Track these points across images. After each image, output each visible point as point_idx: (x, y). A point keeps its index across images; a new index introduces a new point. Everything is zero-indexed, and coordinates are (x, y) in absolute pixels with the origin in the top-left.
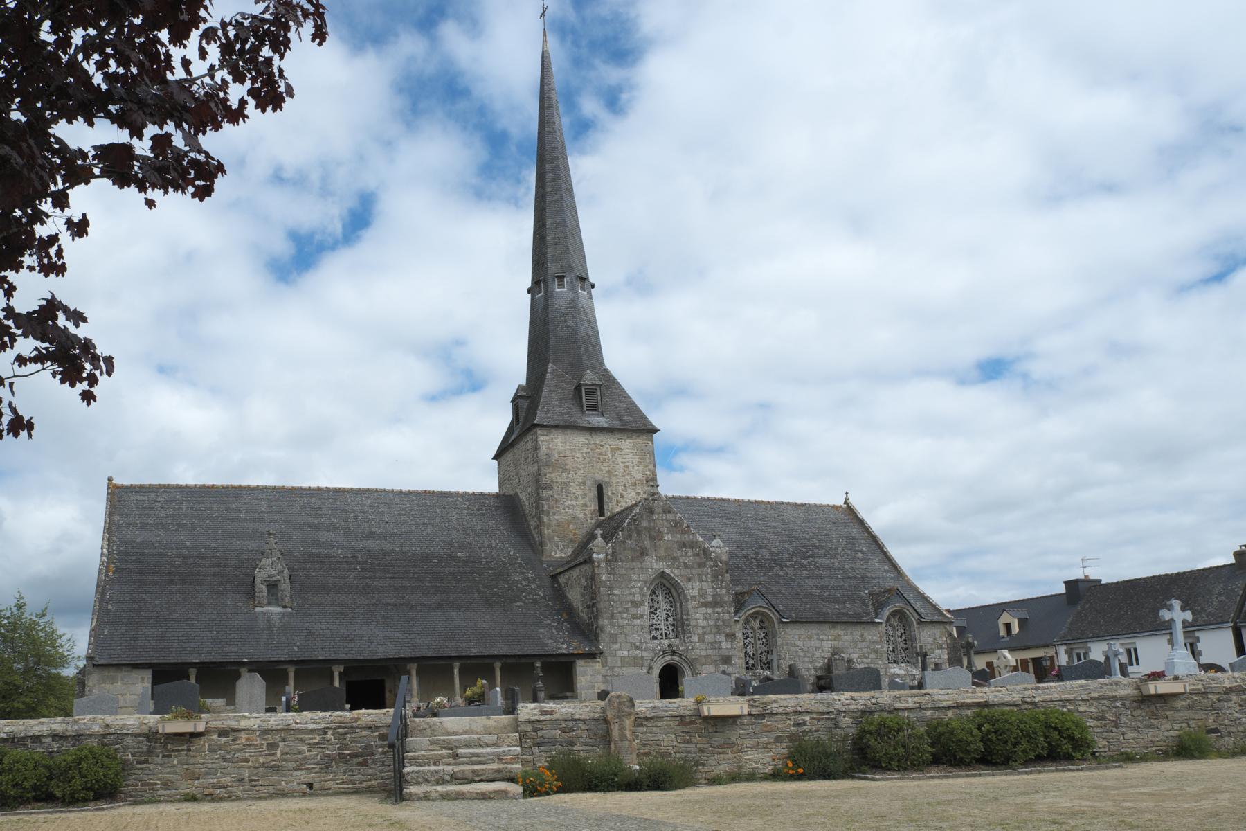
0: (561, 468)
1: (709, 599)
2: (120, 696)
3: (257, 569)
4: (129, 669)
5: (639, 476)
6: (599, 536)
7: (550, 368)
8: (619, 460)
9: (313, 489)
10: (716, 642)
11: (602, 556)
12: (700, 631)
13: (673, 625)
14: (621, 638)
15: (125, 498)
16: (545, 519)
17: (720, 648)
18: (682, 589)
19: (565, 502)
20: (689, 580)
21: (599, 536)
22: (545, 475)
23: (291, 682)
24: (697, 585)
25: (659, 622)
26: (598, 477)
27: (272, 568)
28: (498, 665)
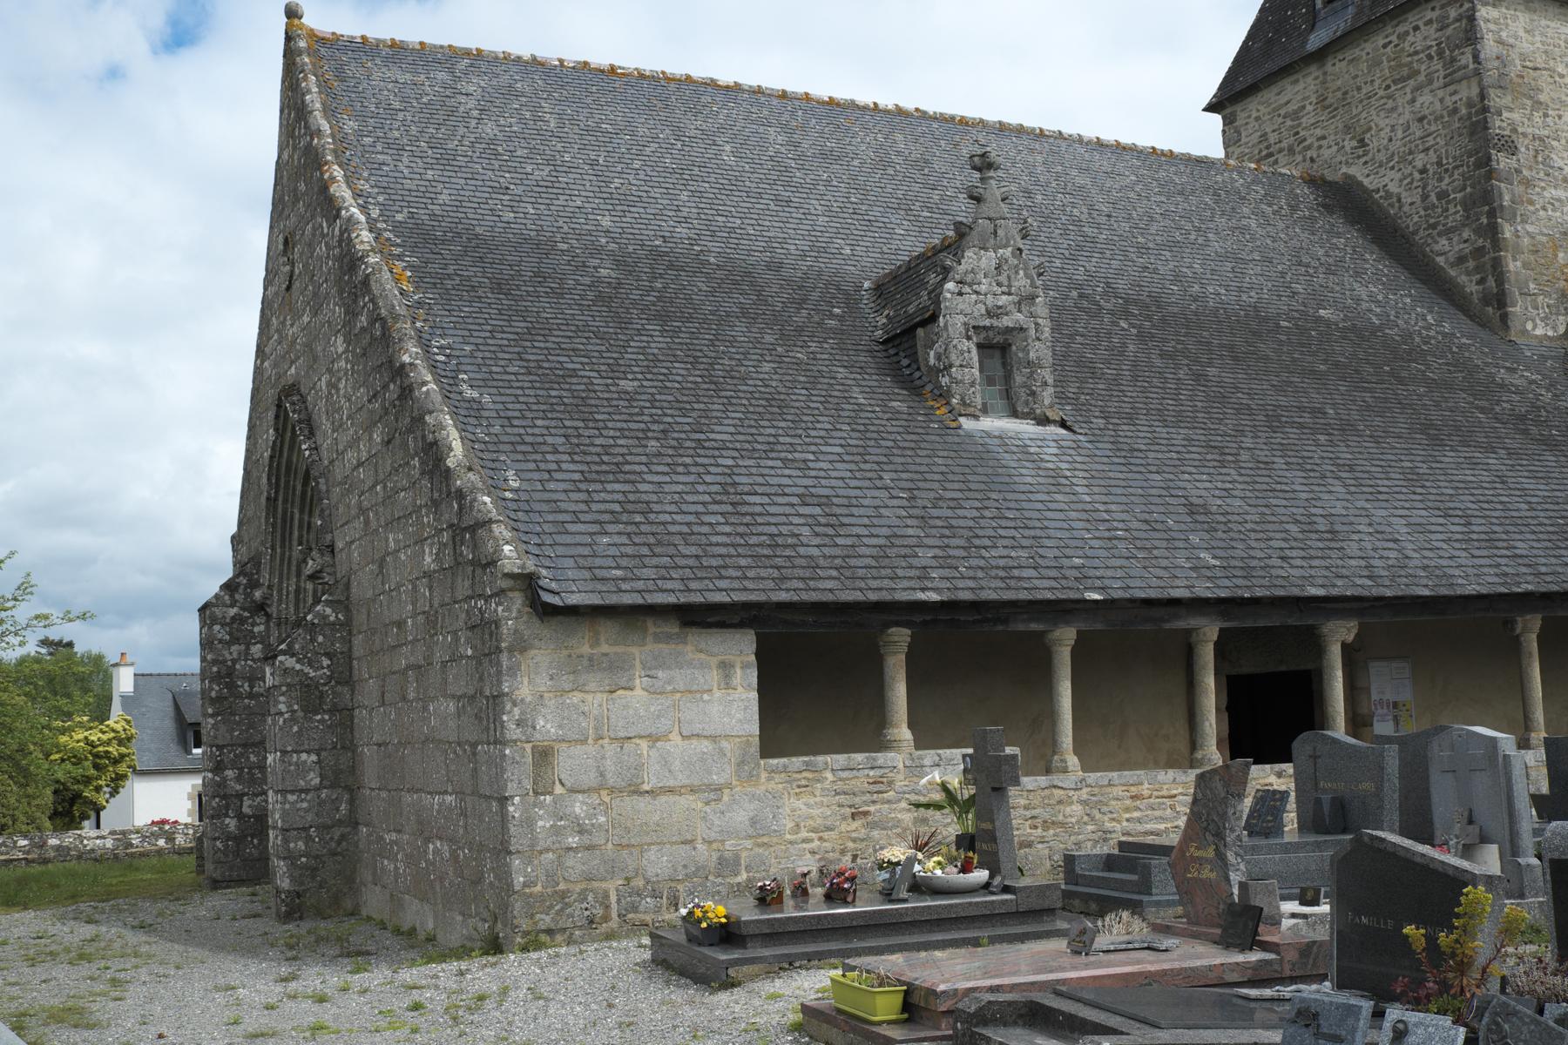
0: (1531, 98)
2: (644, 744)
3: (950, 285)
4: (674, 629)
15: (351, 70)
16: (1507, 232)
19: (1543, 189)
23: (899, 693)
27: (999, 284)
28: (1065, 639)
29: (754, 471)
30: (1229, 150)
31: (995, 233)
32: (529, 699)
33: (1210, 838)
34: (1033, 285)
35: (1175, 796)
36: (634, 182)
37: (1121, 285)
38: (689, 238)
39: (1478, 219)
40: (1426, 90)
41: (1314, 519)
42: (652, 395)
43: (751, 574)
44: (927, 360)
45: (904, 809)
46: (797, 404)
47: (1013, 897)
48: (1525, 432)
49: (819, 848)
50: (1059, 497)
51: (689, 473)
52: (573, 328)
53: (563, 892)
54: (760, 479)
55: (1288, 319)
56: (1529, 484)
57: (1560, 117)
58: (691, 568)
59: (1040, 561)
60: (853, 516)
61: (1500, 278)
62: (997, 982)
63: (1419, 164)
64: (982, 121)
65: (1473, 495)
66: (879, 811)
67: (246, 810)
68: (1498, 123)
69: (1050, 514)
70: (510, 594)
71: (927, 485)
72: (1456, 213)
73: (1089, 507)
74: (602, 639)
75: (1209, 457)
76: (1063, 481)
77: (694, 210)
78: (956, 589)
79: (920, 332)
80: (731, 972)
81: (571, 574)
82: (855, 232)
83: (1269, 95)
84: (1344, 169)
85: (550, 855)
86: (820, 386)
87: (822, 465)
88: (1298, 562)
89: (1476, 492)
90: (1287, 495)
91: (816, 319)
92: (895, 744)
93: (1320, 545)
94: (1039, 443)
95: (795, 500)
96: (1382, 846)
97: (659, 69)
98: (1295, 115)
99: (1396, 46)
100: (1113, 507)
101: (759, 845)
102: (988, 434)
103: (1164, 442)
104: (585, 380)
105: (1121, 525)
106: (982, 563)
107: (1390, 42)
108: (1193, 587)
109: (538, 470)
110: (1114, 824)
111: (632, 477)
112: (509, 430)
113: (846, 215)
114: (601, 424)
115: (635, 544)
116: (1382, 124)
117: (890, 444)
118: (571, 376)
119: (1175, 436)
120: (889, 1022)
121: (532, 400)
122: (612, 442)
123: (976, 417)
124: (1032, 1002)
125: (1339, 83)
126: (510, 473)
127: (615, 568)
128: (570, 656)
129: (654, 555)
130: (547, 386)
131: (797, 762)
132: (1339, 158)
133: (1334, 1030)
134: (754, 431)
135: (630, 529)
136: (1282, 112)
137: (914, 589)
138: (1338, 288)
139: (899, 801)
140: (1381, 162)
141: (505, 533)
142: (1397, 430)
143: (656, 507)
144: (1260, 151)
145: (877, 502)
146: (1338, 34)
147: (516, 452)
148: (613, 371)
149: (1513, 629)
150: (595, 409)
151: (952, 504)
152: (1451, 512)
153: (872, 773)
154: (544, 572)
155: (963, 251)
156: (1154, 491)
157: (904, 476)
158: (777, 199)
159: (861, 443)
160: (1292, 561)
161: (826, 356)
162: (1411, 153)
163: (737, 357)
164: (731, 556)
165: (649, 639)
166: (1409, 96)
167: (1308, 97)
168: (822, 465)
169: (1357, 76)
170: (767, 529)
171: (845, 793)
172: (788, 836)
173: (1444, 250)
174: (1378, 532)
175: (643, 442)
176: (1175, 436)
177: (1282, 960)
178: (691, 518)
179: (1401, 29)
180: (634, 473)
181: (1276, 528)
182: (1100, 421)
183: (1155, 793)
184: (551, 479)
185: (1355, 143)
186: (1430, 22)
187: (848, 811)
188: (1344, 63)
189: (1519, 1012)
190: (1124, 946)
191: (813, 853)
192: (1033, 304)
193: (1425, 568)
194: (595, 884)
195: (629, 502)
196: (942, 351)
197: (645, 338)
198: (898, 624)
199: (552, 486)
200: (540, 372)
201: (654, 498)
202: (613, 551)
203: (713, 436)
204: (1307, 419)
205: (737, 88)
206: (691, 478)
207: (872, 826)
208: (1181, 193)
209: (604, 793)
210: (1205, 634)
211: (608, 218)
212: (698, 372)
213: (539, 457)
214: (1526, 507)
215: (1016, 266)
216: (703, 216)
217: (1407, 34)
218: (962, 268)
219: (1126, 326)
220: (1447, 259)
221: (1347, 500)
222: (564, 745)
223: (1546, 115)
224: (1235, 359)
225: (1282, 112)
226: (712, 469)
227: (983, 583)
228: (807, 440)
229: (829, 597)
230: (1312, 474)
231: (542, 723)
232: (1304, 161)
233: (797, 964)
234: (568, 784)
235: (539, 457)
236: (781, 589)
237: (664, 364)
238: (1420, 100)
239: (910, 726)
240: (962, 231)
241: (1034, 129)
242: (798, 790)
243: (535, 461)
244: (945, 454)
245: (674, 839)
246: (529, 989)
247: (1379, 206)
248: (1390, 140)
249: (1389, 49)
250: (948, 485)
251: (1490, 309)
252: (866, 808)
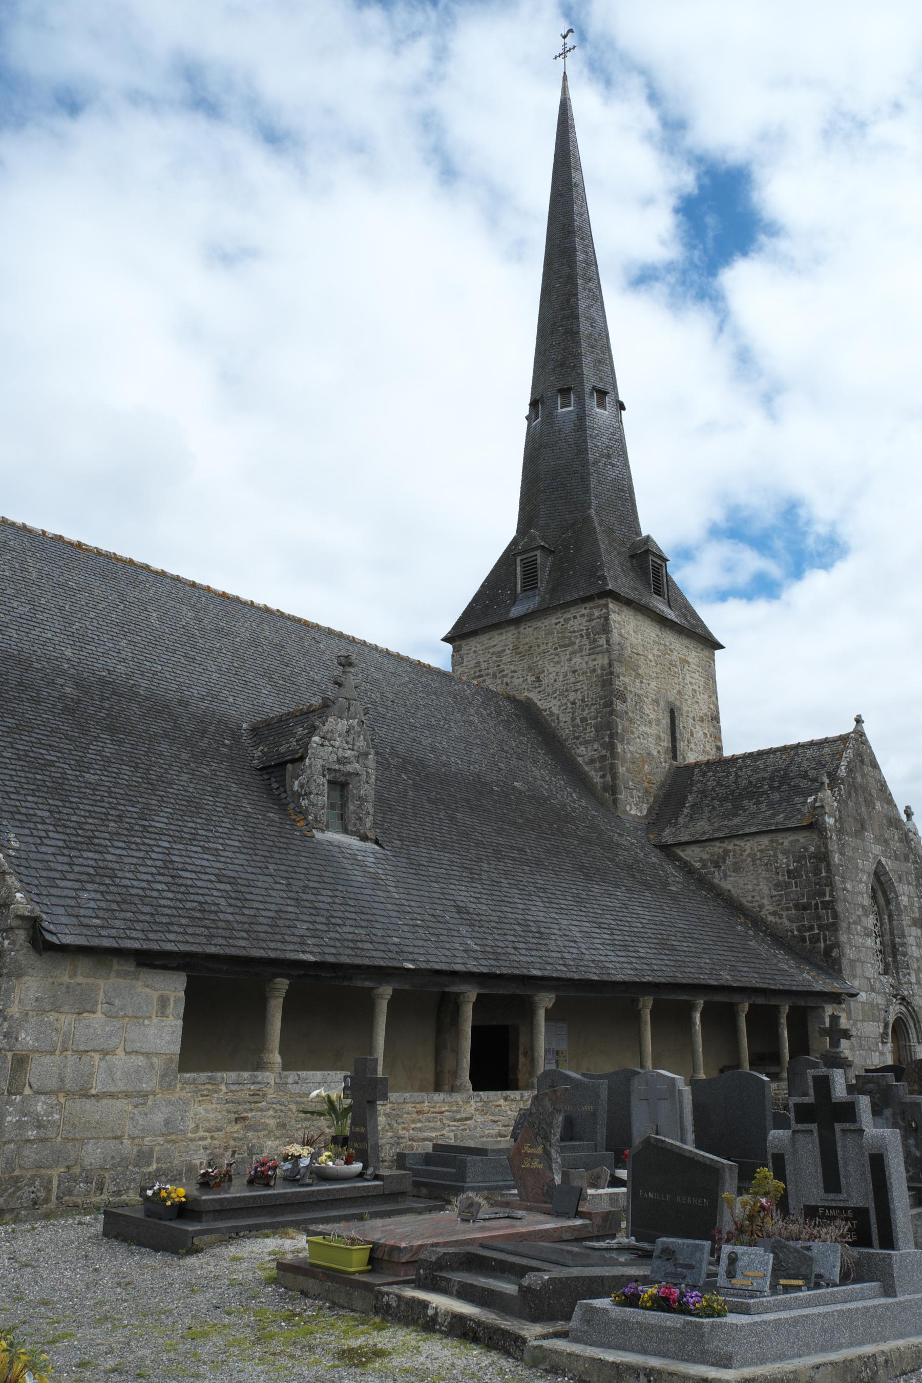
0: (634, 671)
2: (97, 1057)
3: (316, 739)
4: (130, 967)
18: (896, 893)
19: (639, 725)
27: (347, 743)
29: (183, 853)
30: (456, 668)
31: (349, 709)
32: (17, 1016)
33: (539, 1140)
34: (367, 746)
35: (443, 1112)
36: (90, 627)
37: (400, 749)
38: (126, 674)
39: (603, 738)
40: (578, 655)
41: (529, 923)
42: (109, 787)
43: (190, 930)
44: (292, 787)
45: (271, 1116)
46: (207, 807)
47: (381, 1183)
48: (633, 876)
49: (210, 1145)
50: (379, 893)
51: (140, 850)
52: (49, 729)
53: (17, 1177)
54: (188, 860)
55: (498, 786)
56: (640, 911)
57: (649, 684)
58: (148, 922)
59: (373, 937)
60: (252, 893)
61: (614, 776)
62: (436, 1240)
63: (571, 698)
64: (317, 625)
65: (612, 915)
66: (253, 1117)
68: (617, 683)
69: (375, 905)
70: (17, 932)
71: (298, 876)
72: (591, 732)
73: (398, 902)
74: (79, 972)
75: (464, 874)
76: (381, 882)
77: (130, 654)
78: (324, 953)
80: (196, 1241)
81: (64, 920)
82: (236, 688)
83: (484, 639)
84: (526, 694)
85: (12, 1146)
86: (221, 796)
87: (227, 854)
88: (523, 952)
89: (613, 913)
90: (513, 905)
91: (214, 746)
92: (269, 1066)
93: (534, 941)
94: (363, 854)
95: (213, 878)
96: (663, 1146)
97: (112, 551)
98: (499, 654)
99: (563, 625)
100: (413, 904)
101: (169, 1142)
102: (331, 843)
103: (437, 861)
104: (60, 770)
105: (419, 917)
106: (338, 936)
107: (559, 622)
108: (467, 964)
109: (32, 835)
110: (404, 1132)
111: (100, 849)
112: (7, 801)
113: (231, 675)
114: (74, 805)
115: (107, 901)
116: (551, 670)
117: (271, 843)
118: (50, 766)
119: (443, 858)
120: (360, 1272)
121: (23, 780)
122: (83, 820)
123: (323, 831)
124: (469, 1253)
125: (527, 640)
126: (12, 836)
127: (95, 918)
128: (53, 983)
129: (122, 910)
130: (34, 771)
131: (203, 1076)
132: (523, 686)
133: (688, 1261)
134: (180, 823)
135: (102, 888)
136: (491, 651)
137: (298, 951)
138: (524, 769)
139: (268, 1109)
140: (549, 693)
141: (16, 883)
142: (566, 868)
143: (120, 874)
144: (475, 672)
145: (267, 885)
146: (530, 611)
147: (15, 819)
148: (80, 766)
149: (637, 1006)
150: (69, 793)
151: (315, 891)
152: (602, 925)
153: (252, 1088)
154: (44, 916)
155: (327, 717)
156: (435, 895)
157: (282, 868)
158: (186, 656)
159: (252, 840)
160: (521, 951)
161: (223, 774)
162: (567, 691)
163: (165, 766)
164: (175, 916)
165: (113, 974)
166: (568, 657)
167: (508, 645)
168: (227, 854)
169: (537, 639)
170: (196, 898)
171: (233, 1102)
172: (190, 1135)
173: (583, 753)
174: (565, 935)
175: (106, 823)
176: (443, 858)
177: (593, 1224)
178: (144, 885)
179: (567, 616)
180: (101, 845)
181: (508, 926)
182: (398, 842)
183: (432, 1110)
184: (42, 844)
185: (534, 679)
186: (582, 616)
187: (233, 1116)
188: (531, 629)
189: (787, 1245)
190: (494, 1216)
191: (205, 1148)
192: (367, 759)
193: (593, 961)
194: (43, 1171)
195: (100, 867)
196: (305, 782)
197: (100, 744)
198: (282, 976)
199: (43, 849)
200: (28, 759)
201: (117, 866)
202: (92, 904)
203: (153, 824)
204: (515, 855)
205: (163, 574)
206: (141, 854)
207: (248, 1128)
208: (435, 694)
209: (61, 1095)
210: (468, 997)
211: (70, 650)
212: (139, 775)
213: (32, 825)
214: (641, 926)
215: (359, 732)
216: (136, 660)
217: (569, 619)
218: (325, 728)
219: (406, 778)
220: (584, 759)
221: (545, 912)
222: (37, 1055)
223: (642, 682)
224: (471, 808)
225: (491, 651)
226: (155, 849)
227: (341, 951)
228: (217, 834)
229: (243, 953)
230: (524, 892)
231: (23, 1036)
232: (502, 684)
233: (241, 1234)
234: (35, 1086)
235: (32, 825)
236: (211, 944)
237: (115, 765)
238: (574, 660)
239: (280, 1053)
240: (327, 705)
241: (349, 636)
242: (201, 1098)
243: (29, 828)
244: (307, 854)
245: (108, 1135)
246: (10, 1259)
247: (546, 719)
248: (555, 681)
249: (558, 626)
250: (310, 877)
251: (607, 794)
252: (246, 1115)
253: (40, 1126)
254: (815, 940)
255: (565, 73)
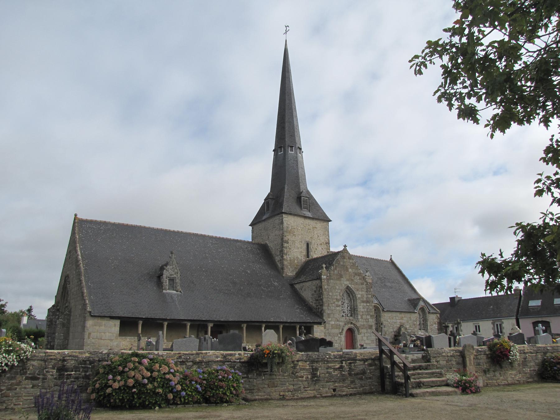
1: (365, 299)
4: (109, 319)
5: (323, 241)
6: (324, 267)
7: (286, 187)
8: (316, 233)
9: (176, 232)
10: (367, 319)
11: (325, 277)
12: (361, 314)
13: (350, 310)
14: (332, 316)
16: (285, 257)
17: (368, 322)
18: (355, 294)
20: (358, 290)
21: (324, 267)
22: (286, 236)
23: (188, 330)
24: (360, 293)
25: (345, 309)
26: (307, 240)
28: (166, 324)
67: (52, 344)
79: (161, 277)
98: (261, 230)
131: (124, 337)
179: (275, 219)
253: (93, 344)
254: (319, 309)
255: (286, 41)
